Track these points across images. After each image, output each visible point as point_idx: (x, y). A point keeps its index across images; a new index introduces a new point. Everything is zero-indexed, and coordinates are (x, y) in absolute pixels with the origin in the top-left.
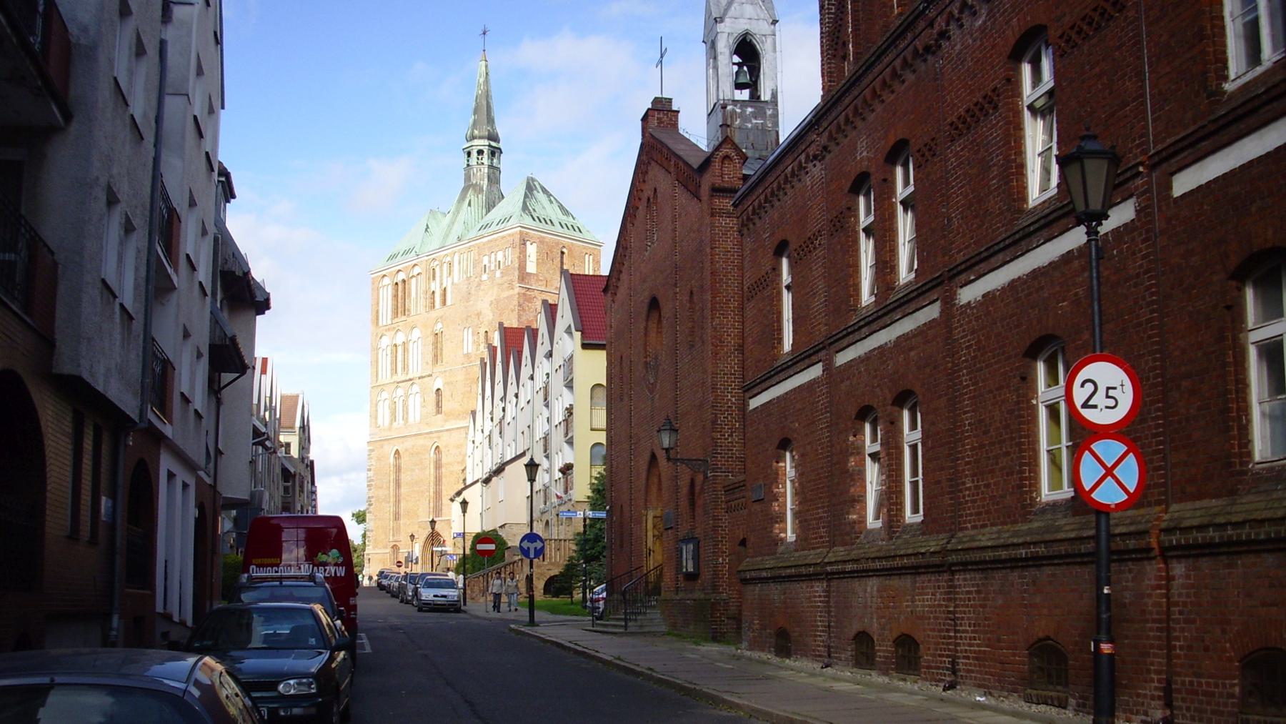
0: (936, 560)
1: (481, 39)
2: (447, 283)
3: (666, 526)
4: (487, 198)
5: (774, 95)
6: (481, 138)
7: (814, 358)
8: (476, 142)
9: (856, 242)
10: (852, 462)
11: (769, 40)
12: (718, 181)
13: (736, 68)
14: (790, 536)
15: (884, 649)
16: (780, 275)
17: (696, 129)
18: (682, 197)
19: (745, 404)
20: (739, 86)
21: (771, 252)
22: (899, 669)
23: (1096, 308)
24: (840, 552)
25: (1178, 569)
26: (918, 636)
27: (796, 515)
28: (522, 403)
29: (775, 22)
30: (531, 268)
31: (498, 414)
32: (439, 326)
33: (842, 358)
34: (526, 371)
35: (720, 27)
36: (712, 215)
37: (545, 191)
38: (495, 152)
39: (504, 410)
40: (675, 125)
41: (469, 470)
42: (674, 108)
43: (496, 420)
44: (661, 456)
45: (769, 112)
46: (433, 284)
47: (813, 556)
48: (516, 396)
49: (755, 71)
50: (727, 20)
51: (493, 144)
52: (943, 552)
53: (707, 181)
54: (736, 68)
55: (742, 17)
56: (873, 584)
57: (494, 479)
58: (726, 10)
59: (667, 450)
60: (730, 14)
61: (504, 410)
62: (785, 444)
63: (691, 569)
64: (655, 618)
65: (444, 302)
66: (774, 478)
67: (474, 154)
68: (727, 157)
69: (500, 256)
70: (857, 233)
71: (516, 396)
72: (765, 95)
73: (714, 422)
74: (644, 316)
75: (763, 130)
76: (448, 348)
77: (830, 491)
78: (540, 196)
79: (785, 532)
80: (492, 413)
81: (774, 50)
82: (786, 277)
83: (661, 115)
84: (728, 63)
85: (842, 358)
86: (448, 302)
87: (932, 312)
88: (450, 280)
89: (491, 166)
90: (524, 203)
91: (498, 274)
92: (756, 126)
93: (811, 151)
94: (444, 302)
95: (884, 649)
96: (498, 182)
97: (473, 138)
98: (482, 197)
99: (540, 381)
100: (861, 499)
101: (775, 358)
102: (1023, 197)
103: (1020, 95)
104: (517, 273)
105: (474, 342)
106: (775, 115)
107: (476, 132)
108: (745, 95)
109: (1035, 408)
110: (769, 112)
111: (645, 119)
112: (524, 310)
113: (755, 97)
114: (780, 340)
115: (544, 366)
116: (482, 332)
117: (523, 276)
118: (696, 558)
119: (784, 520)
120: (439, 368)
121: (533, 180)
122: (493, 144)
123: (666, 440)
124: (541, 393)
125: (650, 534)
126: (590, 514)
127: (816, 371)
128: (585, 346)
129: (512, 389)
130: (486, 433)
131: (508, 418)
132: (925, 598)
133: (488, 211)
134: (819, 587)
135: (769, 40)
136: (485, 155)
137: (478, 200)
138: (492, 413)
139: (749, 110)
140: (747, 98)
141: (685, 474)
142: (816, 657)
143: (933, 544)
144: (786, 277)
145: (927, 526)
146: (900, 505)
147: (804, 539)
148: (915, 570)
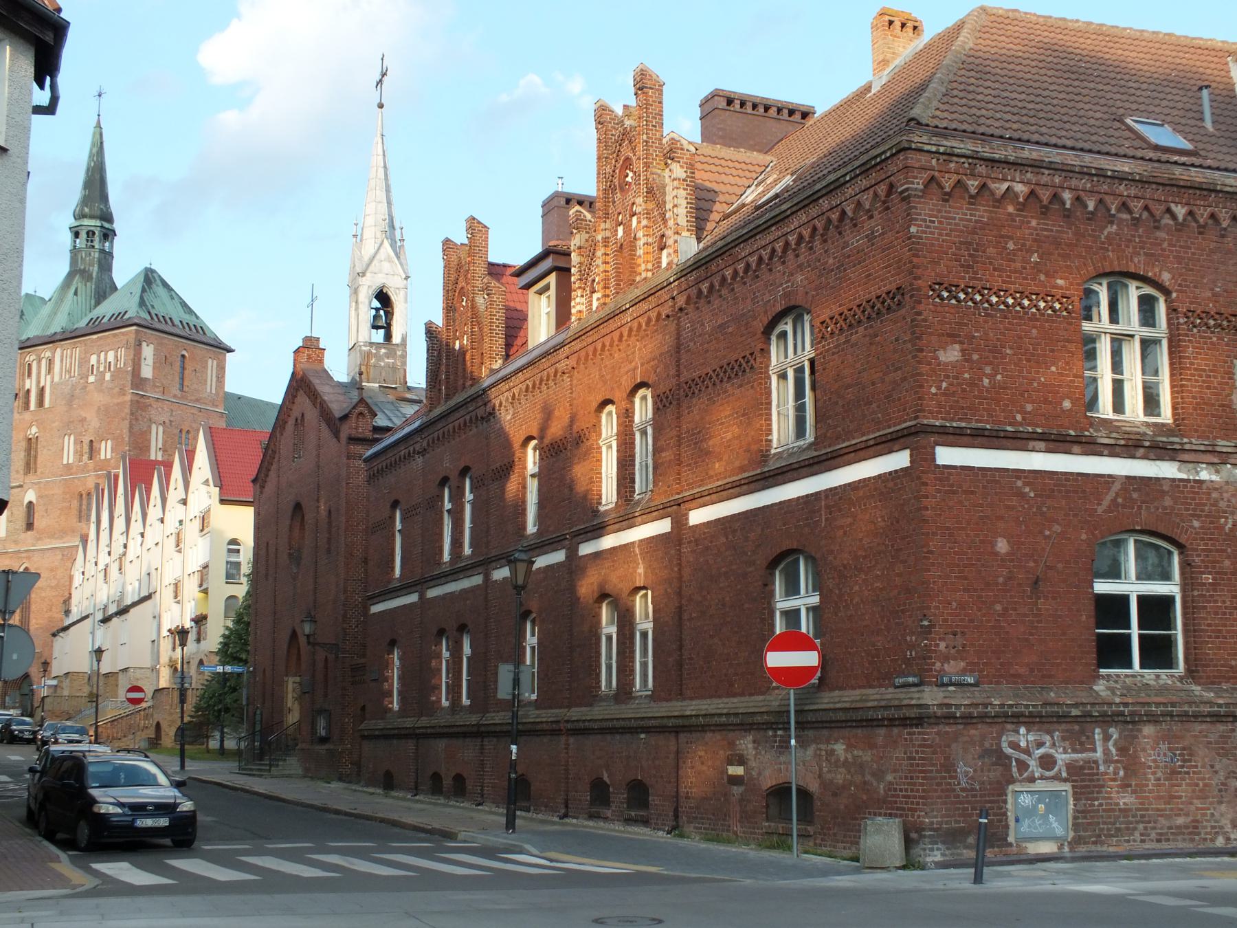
0: (475, 729)
1: (95, 101)
2: (46, 381)
3: (306, 693)
4: (97, 287)
5: (404, 339)
6: (92, 217)
7: (414, 589)
8: (86, 222)
9: (442, 519)
10: (433, 663)
11: (402, 293)
12: (353, 433)
13: (373, 312)
14: (396, 706)
15: (447, 782)
16: (394, 521)
17: (339, 367)
18: (326, 432)
19: (366, 609)
20: (375, 327)
21: (388, 505)
22: (433, 793)
23: (1125, 167)
24: (424, 721)
25: (572, 740)
26: (465, 775)
27: (400, 693)
28: (149, 541)
29: (407, 278)
30: (147, 372)
31: (117, 549)
32: (34, 430)
33: (432, 593)
34: (154, 512)
35: (362, 281)
36: (348, 458)
37: (165, 285)
38: (108, 235)
39: (125, 546)
40: (321, 361)
41: (74, 601)
42: (321, 346)
43: (115, 555)
44: (302, 640)
45: (399, 353)
46: (28, 382)
47: (409, 722)
48: (142, 535)
49: (389, 315)
50: (368, 274)
51: (106, 225)
52: (478, 725)
53: (346, 431)
54: (373, 312)
55: (380, 272)
56: (441, 744)
57: (115, 620)
58: (368, 266)
59: (308, 636)
60: (371, 268)
61: (125, 546)
62: (393, 643)
63: (323, 733)
64: (293, 764)
65: (41, 403)
66: (387, 665)
67: (83, 235)
68: (361, 414)
69: (111, 356)
70: (442, 512)
71: (142, 535)
72: (396, 339)
73: (345, 616)
74: (290, 514)
75: (394, 368)
76: (43, 455)
77: (419, 681)
78: (160, 290)
79: (392, 703)
80: (110, 545)
81: (406, 301)
82: (398, 526)
83: (310, 349)
84: (368, 306)
85: (432, 593)
86: (47, 404)
87: (477, 580)
88: (49, 377)
89: (102, 251)
90: (142, 298)
91: (108, 376)
92: (388, 365)
93: (417, 447)
94: (41, 403)
95: (447, 782)
96: (110, 269)
97: (83, 216)
98: (91, 286)
99: (171, 525)
100: (439, 687)
101: (390, 581)
102: (525, 528)
103: (525, 468)
104: (129, 378)
105: (75, 452)
106: (404, 356)
107: (86, 210)
108: (379, 336)
109: (525, 648)
110: (399, 353)
111: (296, 352)
112: (137, 419)
113: (388, 337)
114: (393, 568)
115: (175, 512)
116: (86, 440)
117: (138, 381)
118: (329, 728)
119: (391, 695)
120: (31, 478)
121: (153, 271)
122: (106, 225)
123: (307, 628)
124: (173, 539)
125: (290, 696)
126: (220, 669)
127: (413, 598)
128: (223, 502)
129: (136, 527)
130: (101, 566)
131: (131, 554)
132: (468, 752)
133: (98, 303)
134: (411, 744)
135: (402, 293)
136: (97, 238)
137: (86, 290)
138: (110, 545)
139: (383, 351)
140: (381, 340)
141: (321, 654)
142: (409, 790)
143: (474, 719)
144: (398, 526)
145: (471, 709)
146: (460, 693)
147: (403, 712)
148: (465, 735)
